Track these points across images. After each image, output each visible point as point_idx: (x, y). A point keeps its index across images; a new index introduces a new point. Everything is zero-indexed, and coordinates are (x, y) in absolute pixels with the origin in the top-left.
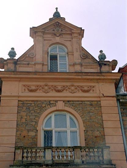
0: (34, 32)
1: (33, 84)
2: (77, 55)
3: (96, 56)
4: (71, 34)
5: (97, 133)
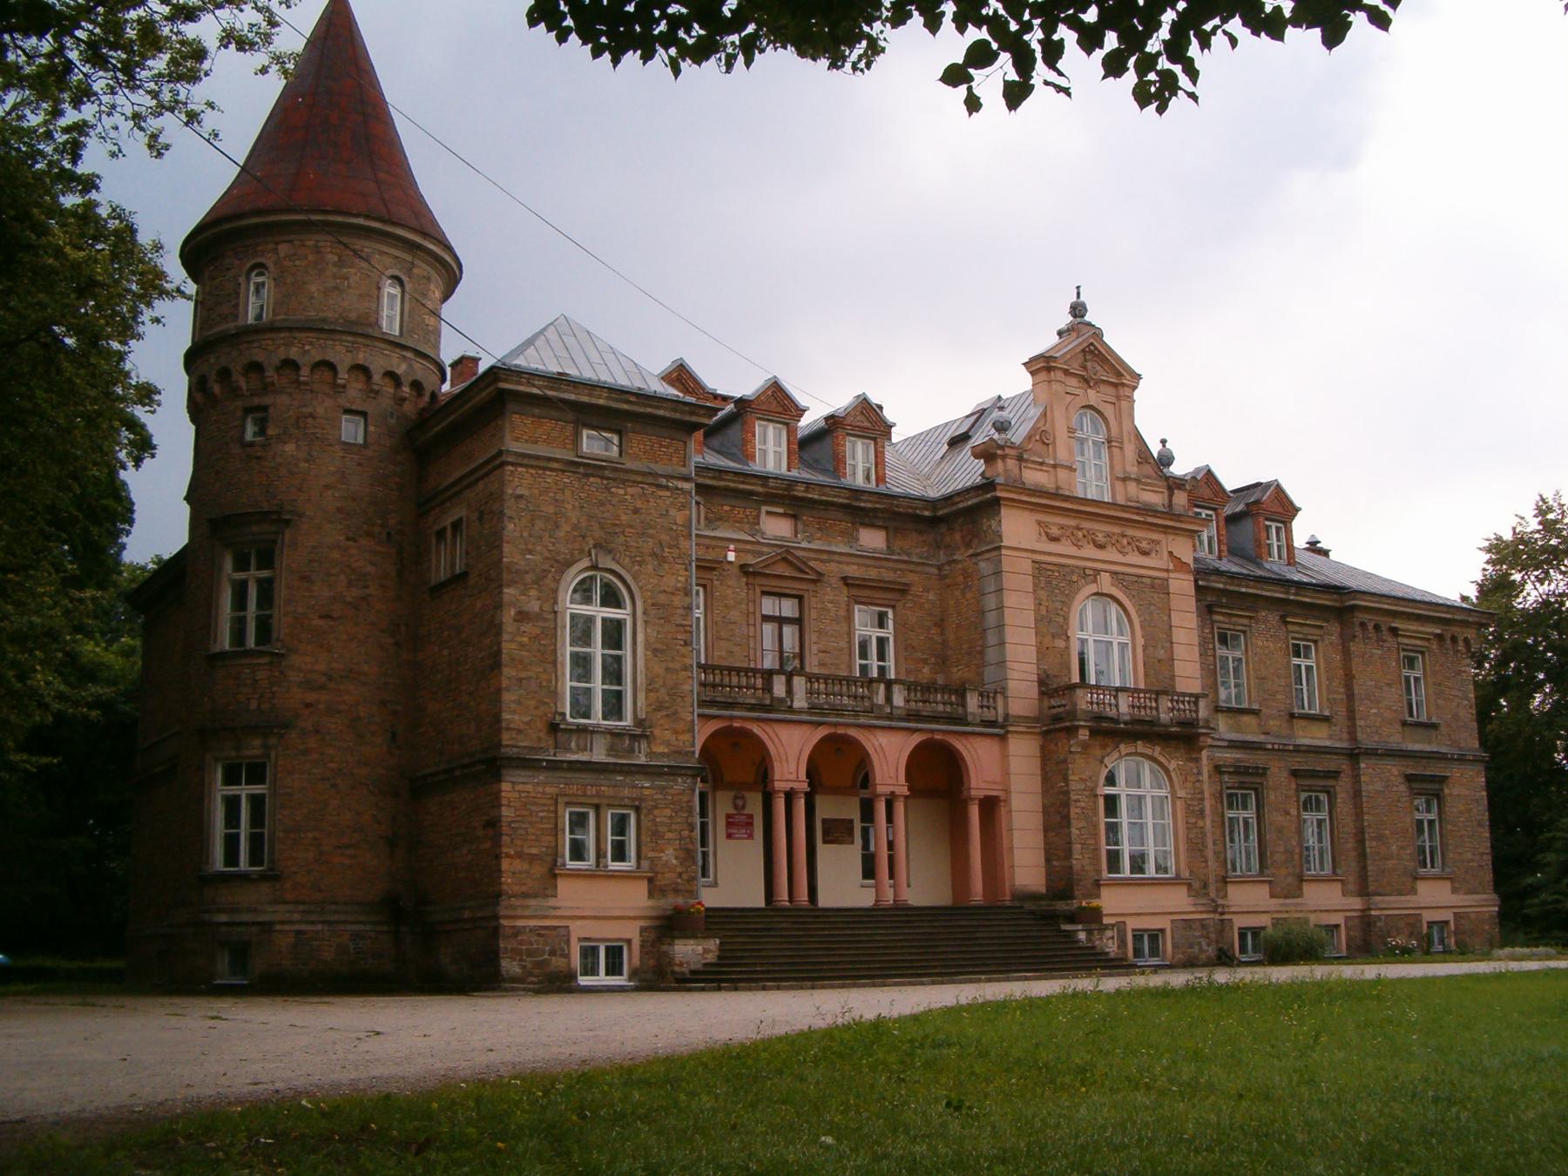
0: (1041, 366)
2: (1130, 450)
3: (1155, 449)
4: (1115, 385)
5: (1161, 653)
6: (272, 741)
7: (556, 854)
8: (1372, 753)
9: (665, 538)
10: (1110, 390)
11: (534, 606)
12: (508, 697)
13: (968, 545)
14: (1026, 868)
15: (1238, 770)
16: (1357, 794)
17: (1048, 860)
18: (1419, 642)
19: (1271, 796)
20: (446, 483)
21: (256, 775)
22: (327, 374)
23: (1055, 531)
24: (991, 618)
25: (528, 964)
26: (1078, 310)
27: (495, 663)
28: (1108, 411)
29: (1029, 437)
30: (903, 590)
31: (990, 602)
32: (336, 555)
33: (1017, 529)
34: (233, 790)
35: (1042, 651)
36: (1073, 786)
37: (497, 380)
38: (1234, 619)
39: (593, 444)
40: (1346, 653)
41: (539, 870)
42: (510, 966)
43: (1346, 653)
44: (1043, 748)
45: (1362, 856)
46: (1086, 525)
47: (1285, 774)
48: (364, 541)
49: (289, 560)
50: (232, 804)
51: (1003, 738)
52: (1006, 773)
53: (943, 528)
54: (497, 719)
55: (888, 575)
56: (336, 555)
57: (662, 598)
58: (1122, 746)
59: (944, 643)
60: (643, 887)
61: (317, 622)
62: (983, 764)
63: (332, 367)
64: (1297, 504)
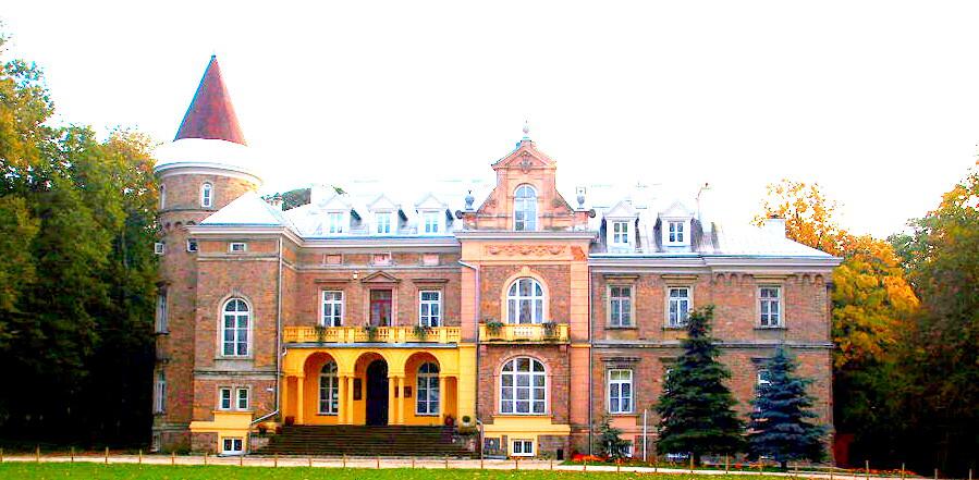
1: (496, 246)
5: (563, 303)
7: (214, 404)
10: (541, 172)
11: (209, 314)
14: (465, 406)
18: (776, 281)
23: (496, 250)
25: (202, 445)
30: (447, 281)
38: (623, 281)
42: (195, 446)
46: (515, 244)
47: (656, 360)
52: (458, 367)
57: (263, 306)
58: (512, 353)
60: (250, 417)
62: (447, 364)
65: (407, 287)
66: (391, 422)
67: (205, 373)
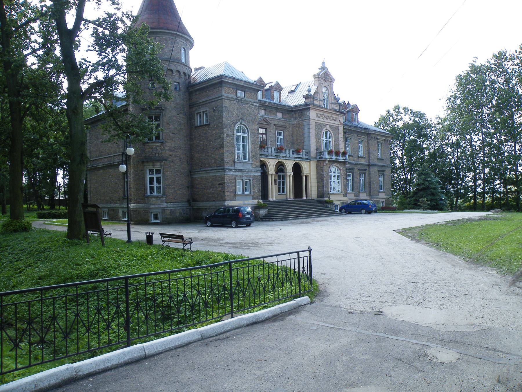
6: (162, 164)
8: (372, 165)
9: (254, 117)
11: (230, 133)
12: (225, 155)
13: (300, 118)
15: (350, 169)
16: (369, 174)
17: (318, 189)
19: (355, 175)
20: (201, 101)
21: (158, 172)
22: (171, 72)
24: (306, 135)
26: (323, 64)
27: (222, 146)
28: (328, 87)
29: (315, 93)
30: (285, 127)
31: (306, 131)
32: (175, 118)
33: (312, 114)
34: (152, 176)
35: (317, 143)
36: (324, 173)
37: (222, 78)
39: (240, 94)
40: (368, 143)
41: (232, 195)
43: (368, 143)
44: (317, 164)
45: (370, 188)
48: (181, 115)
49: (164, 119)
50: (151, 179)
51: (309, 162)
52: (310, 170)
53: (293, 113)
54: (223, 160)
55: (283, 124)
56: (175, 118)
59: (293, 139)
61: (171, 135)
63: (172, 71)
64: (282, 87)
65: (272, 125)
66: (270, 199)
67: (230, 170)
